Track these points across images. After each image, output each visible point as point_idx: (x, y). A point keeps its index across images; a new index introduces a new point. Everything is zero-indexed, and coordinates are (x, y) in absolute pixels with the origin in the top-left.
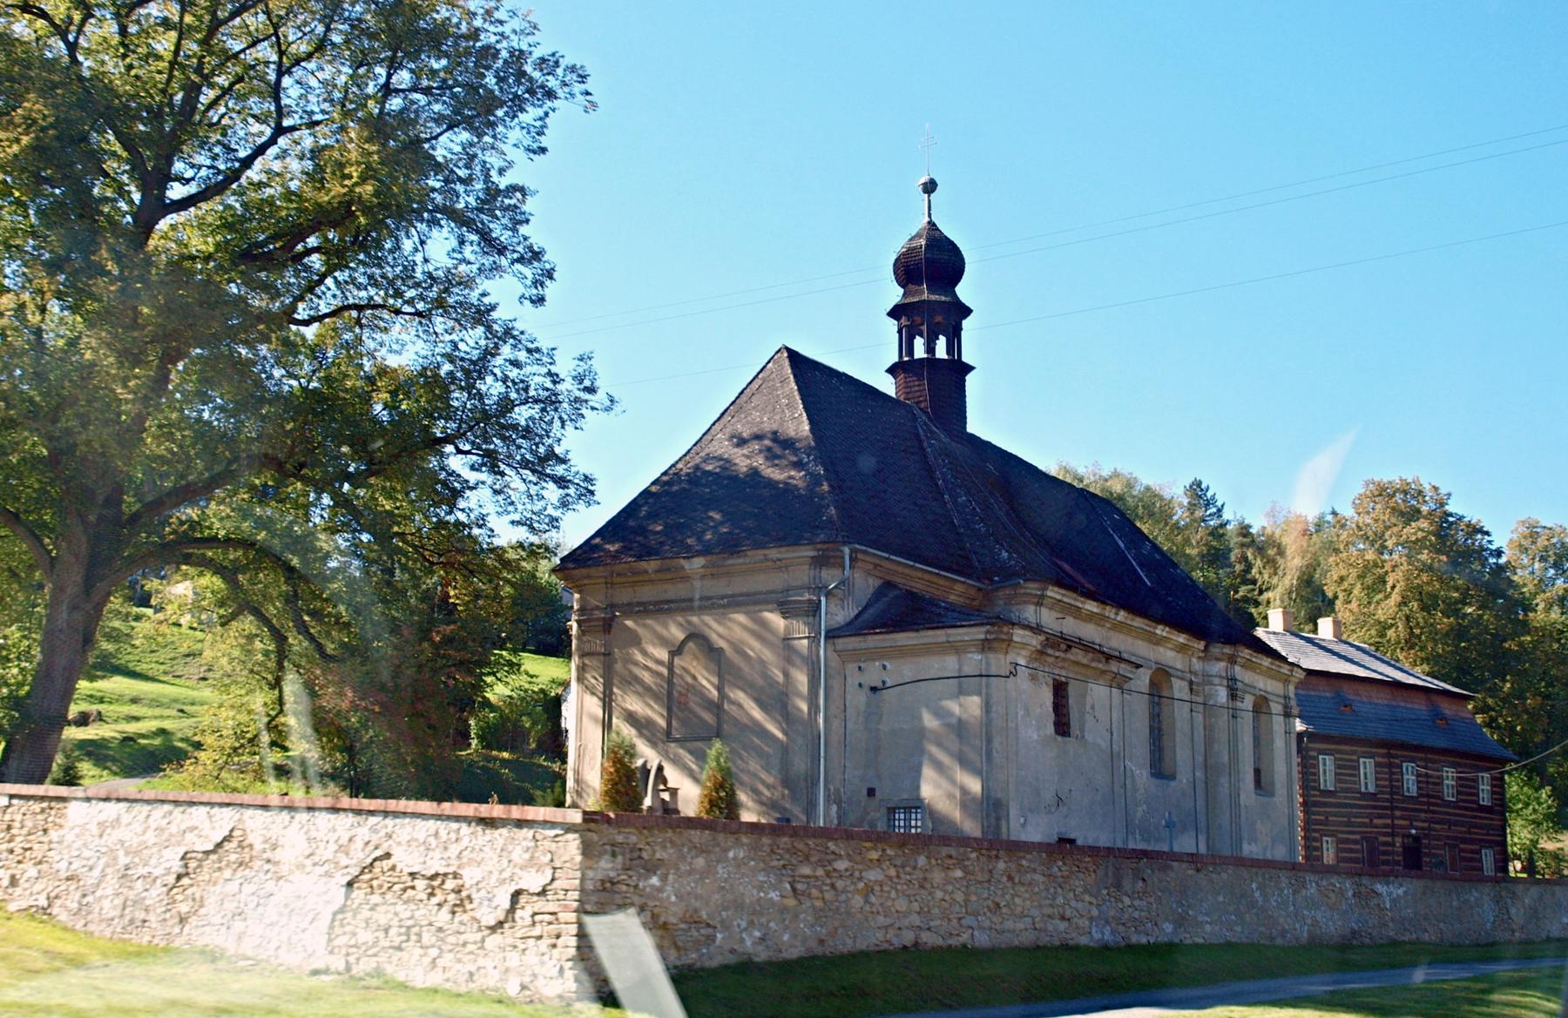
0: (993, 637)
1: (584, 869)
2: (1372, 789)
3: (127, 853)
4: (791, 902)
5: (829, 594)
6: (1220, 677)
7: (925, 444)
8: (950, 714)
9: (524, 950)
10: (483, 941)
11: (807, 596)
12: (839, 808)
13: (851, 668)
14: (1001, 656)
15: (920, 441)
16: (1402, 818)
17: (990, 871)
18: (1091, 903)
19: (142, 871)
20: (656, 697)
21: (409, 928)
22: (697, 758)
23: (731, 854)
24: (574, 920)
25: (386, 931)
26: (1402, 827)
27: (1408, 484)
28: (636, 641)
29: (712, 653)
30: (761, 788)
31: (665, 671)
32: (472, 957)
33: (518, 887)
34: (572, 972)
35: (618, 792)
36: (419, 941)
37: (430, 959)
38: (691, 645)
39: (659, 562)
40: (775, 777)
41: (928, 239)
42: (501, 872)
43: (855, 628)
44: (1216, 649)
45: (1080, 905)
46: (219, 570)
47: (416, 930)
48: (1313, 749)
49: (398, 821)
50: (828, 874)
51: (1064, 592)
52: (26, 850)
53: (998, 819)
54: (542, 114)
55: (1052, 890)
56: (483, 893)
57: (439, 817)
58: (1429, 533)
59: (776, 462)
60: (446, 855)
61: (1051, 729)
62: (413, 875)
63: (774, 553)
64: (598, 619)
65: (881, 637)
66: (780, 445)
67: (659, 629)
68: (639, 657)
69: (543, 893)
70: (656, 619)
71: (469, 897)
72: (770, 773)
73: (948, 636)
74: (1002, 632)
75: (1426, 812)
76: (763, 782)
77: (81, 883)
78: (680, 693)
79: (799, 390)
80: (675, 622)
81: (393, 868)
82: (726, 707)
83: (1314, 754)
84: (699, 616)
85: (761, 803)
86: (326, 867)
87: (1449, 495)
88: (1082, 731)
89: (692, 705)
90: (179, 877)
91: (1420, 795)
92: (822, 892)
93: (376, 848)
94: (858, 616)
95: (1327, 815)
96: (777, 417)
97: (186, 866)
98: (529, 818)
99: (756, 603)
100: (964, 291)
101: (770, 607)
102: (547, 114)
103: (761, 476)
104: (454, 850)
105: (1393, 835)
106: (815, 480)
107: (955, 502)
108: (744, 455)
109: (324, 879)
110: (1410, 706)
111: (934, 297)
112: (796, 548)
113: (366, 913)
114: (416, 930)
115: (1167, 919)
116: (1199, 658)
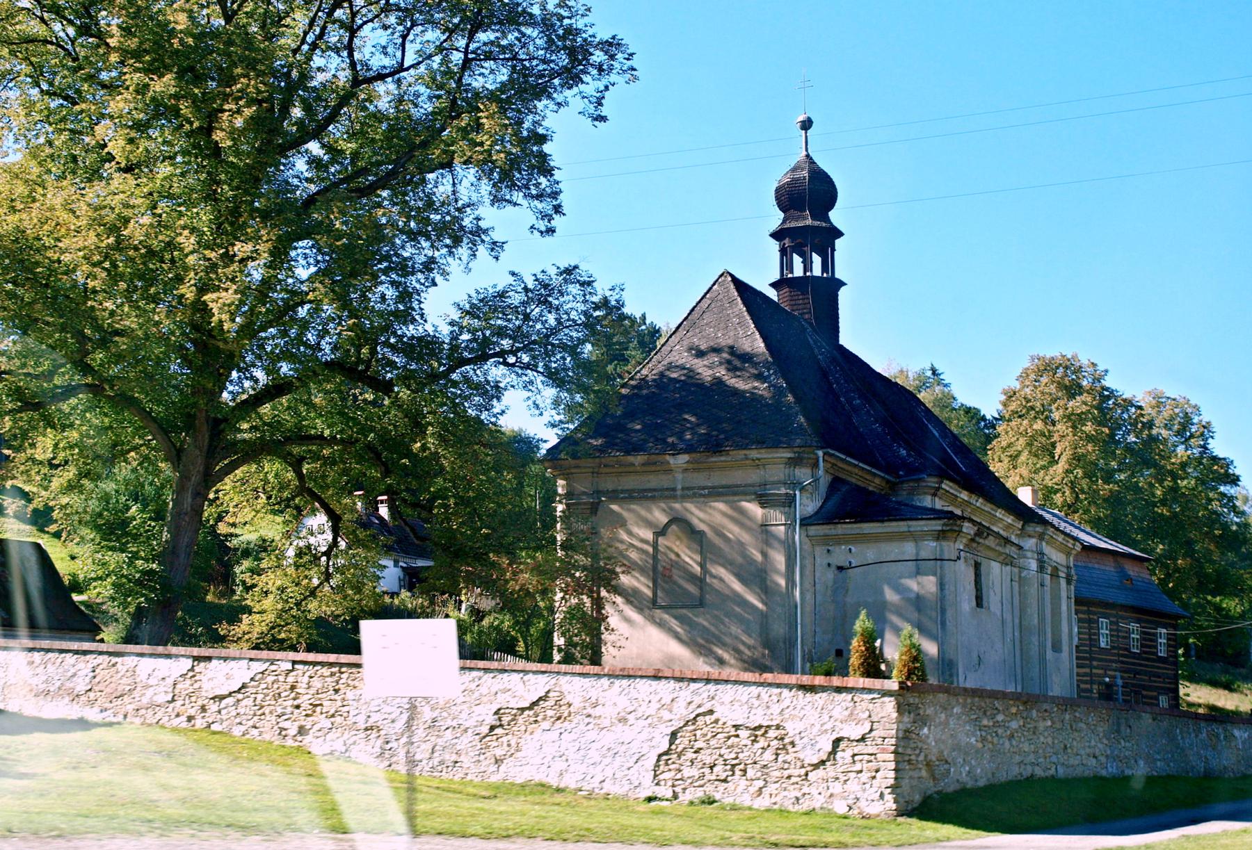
1: (899, 722)
3: (433, 709)
4: (980, 745)
5: (802, 489)
6: (1032, 551)
8: (909, 590)
9: (846, 781)
10: (807, 775)
11: (783, 491)
14: (952, 544)
19: (449, 723)
20: (642, 570)
21: (734, 766)
22: (681, 623)
24: (892, 759)
26: (1099, 676)
27: (1069, 360)
28: (622, 523)
29: (694, 535)
30: (742, 648)
31: (650, 550)
32: (796, 786)
34: (891, 796)
35: (869, 664)
37: (757, 788)
38: (674, 527)
39: (646, 457)
40: (755, 640)
41: (809, 172)
42: (822, 725)
47: (742, 767)
49: (719, 686)
51: (951, 484)
52: (316, 706)
53: (951, 675)
54: (602, 88)
56: (806, 740)
57: (761, 684)
58: (1092, 406)
59: (738, 373)
60: (769, 712)
62: (737, 727)
63: (754, 454)
64: (585, 504)
65: (850, 526)
66: (738, 359)
67: (643, 513)
68: (625, 537)
69: (863, 739)
70: (641, 505)
71: (793, 744)
72: (750, 636)
73: (909, 527)
74: (956, 525)
76: (744, 643)
77: (382, 733)
78: (664, 567)
79: (748, 311)
80: (659, 507)
82: (708, 580)
84: (681, 502)
85: (744, 661)
86: (649, 720)
87: (1106, 371)
89: (676, 578)
90: (492, 728)
91: (1113, 648)
93: (699, 706)
94: (821, 507)
96: (732, 334)
97: (500, 719)
98: (849, 686)
99: (735, 494)
100: (835, 217)
101: (748, 497)
102: (607, 88)
103: (727, 386)
105: (1092, 682)
106: (778, 392)
107: (850, 403)
108: (705, 366)
110: (1103, 567)
111: (817, 223)
112: (774, 450)
114: (742, 767)
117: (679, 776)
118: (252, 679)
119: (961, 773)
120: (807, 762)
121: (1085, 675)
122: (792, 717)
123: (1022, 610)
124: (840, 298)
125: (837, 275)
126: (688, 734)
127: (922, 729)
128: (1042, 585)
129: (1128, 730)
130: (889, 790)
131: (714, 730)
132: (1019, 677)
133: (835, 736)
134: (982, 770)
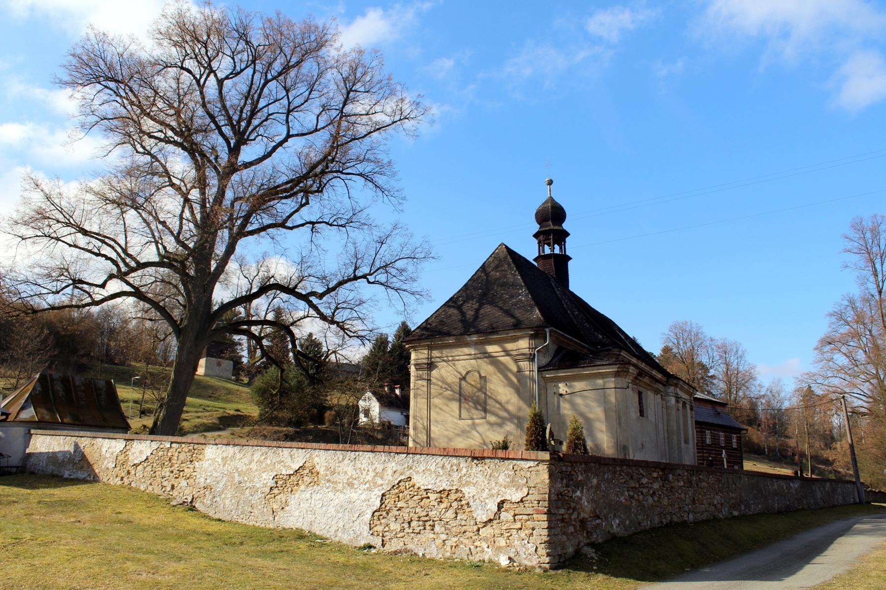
3: (239, 475)
10: (478, 530)
15: (554, 289)
16: (706, 453)
33: (503, 499)
36: (433, 530)
47: (430, 522)
51: (626, 353)
74: (625, 367)
75: (715, 450)
81: (413, 486)
86: (367, 485)
91: (712, 444)
97: (276, 483)
100: (566, 226)
104: (455, 476)
107: (573, 314)
113: (395, 512)
117: (387, 529)
118: (152, 454)
119: (612, 526)
120: (478, 520)
121: (701, 456)
122: (468, 484)
123: (668, 421)
125: (567, 253)
126: (393, 497)
127: (574, 491)
128: (678, 410)
129: (734, 486)
130: (543, 545)
131: (411, 493)
133: (499, 500)
134: (630, 522)
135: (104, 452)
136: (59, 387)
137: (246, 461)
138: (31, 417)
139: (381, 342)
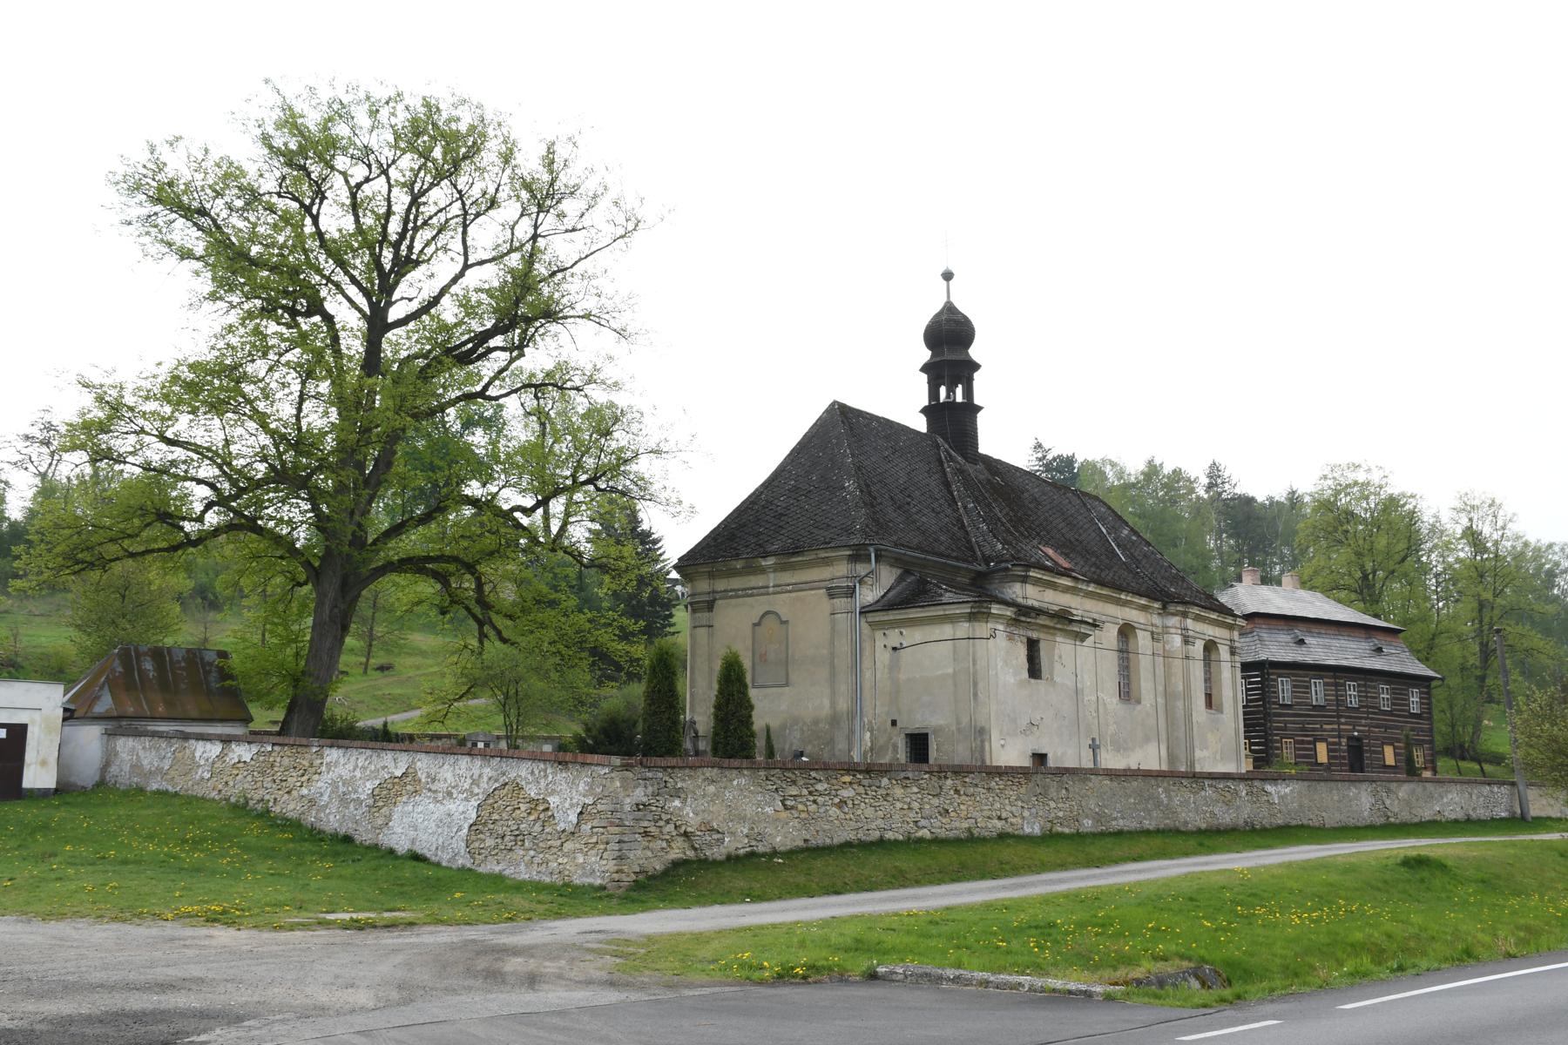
0: (976, 610)
2: (1322, 703)
3: (343, 785)
7: (946, 465)
12: (872, 734)
13: (879, 634)
14: (984, 624)
17: (940, 787)
18: (1022, 807)
23: (735, 783)
25: (503, 837)
43: (889, 604)
44: (1172, 608)
45: (1014, 808)
46: (436, 575)
48: (1273, 674)
50: (810, 793)
53: (983, 742)
55: (991, 799)
61: (1025, 674)
63: (823, 554)
83: (1274, 677)
88: (1052, 674)
92: (807, 806)
94: (883, 597)
95: (1286, 723)
105: (1339, 737)
109: (464, 803)
115: (1087, 817)
116: (1159, 614)
122: (553, 792)
124: (978, 420)
132: (1163, 736)
135: (197, 759)
136: (148, 665)
137: (350, 766)
138: (107, 711)
139: (110, 734)
